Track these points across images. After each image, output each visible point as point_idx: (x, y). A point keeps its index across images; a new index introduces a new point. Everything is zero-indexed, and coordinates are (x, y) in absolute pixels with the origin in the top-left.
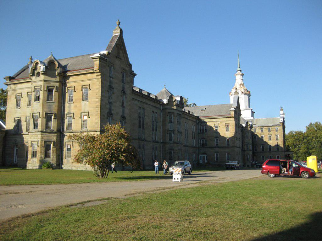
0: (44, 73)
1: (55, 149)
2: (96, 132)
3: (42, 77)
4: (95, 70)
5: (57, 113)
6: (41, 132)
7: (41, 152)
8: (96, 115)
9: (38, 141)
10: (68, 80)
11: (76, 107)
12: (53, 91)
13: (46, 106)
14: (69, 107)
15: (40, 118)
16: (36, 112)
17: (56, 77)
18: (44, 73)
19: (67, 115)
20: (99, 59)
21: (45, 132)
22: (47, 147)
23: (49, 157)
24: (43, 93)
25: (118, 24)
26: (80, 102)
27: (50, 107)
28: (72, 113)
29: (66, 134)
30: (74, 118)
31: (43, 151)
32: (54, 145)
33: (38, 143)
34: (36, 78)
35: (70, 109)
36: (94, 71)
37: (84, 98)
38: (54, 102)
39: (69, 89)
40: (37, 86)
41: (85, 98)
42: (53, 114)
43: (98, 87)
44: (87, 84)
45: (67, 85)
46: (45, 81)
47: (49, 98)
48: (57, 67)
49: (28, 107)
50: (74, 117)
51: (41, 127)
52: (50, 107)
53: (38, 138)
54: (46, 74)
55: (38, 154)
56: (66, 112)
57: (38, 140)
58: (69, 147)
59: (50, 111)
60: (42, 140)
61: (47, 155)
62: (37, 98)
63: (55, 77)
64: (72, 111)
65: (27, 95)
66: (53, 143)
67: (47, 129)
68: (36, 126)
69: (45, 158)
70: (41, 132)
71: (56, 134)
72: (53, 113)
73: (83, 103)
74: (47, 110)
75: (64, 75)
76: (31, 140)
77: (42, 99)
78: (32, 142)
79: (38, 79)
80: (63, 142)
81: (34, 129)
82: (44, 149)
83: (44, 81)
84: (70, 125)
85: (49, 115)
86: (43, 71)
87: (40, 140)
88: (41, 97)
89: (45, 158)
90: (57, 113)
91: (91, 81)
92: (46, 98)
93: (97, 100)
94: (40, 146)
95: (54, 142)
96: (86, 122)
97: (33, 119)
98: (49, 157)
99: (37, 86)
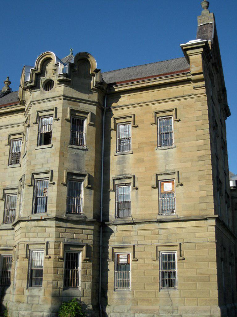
0: (65, 78)
1: (89, 264)
2: (206, 219)
3: (59, 89)
4: (193, 75)
5: (93, 175)
6: (57, 219)
7: (56, 273)
8: (201, 178)
9: (48, 243)
10: (116, 102)
11: (140, 161)
12: (83, 125)
13: (68, 155)
14: (122, 162)
15: (54, 184)
16: (43, 171)
17: (92, 93)
18: (65, 78)
19: (117, 182)
20: (201, 50)
21: (67, 221)
22: (70, 261)
23: (74, 287)
24: (62, 126)
25: (206, 5)
26: (152, 150)
27: (77, 160)
28: (129, 176)
29: (114, 228)
30: (137, 189)
31: (61, 271)
32: (88, 254)
33: (47, 249)
34: (42, 92)
35: (124, 167)
36: (189, 77)
37: (161, 141)
38: (87, 150)
39: (118, 121)
40: (45, 111)
41: (165, 140)
42: (84, 176)
43: (200, 113)
44: (171, 108)
45: (113, 112)
46: (66, 97)
47: (74, 139)
48: (94, 70)
49: (10, 166)
50: (136, 185)
51: (57, 207)
52: (77, 160)
53: (45, 234)
54: (69, 81)
55: (48, 278)
56: (112, 176)
57: (47, 240)
58: (123, 260)
59: (78, 168)
60: (59, 240)
61: (69, 280)
62: (46, 139)
63: (88, 91)
64: (130, 171)
65: (7, 141)
66: (84, 248)
67: (68, 216)
68: (38, 204)
69: (64, 289)
70: (57, 219)
71: (92, 227)
72: (84, 173)
73: (160, 153)
74: (70, 166)
75: (108, 94)
76: (27, 240)
77: (59, 138)
78: (30, 247)
79: (48, 94)
80: (108, 247)
81: (36, 212)
82: (62, 263)
83: (64, 99)
84: (123, 206)
85: (74, 177)
86: (65, 75)
87: (52, 240)
88: (56, 135)
89: (64, 289)
90: (93, 175)
91: (178, 102)
92: (69, 141)
93: (201, 142)
94: (52, 257)
95: (88, 247)
96: (169, 198)
97: (33, 187)
98: (76, 286)
99: (45, 111)
